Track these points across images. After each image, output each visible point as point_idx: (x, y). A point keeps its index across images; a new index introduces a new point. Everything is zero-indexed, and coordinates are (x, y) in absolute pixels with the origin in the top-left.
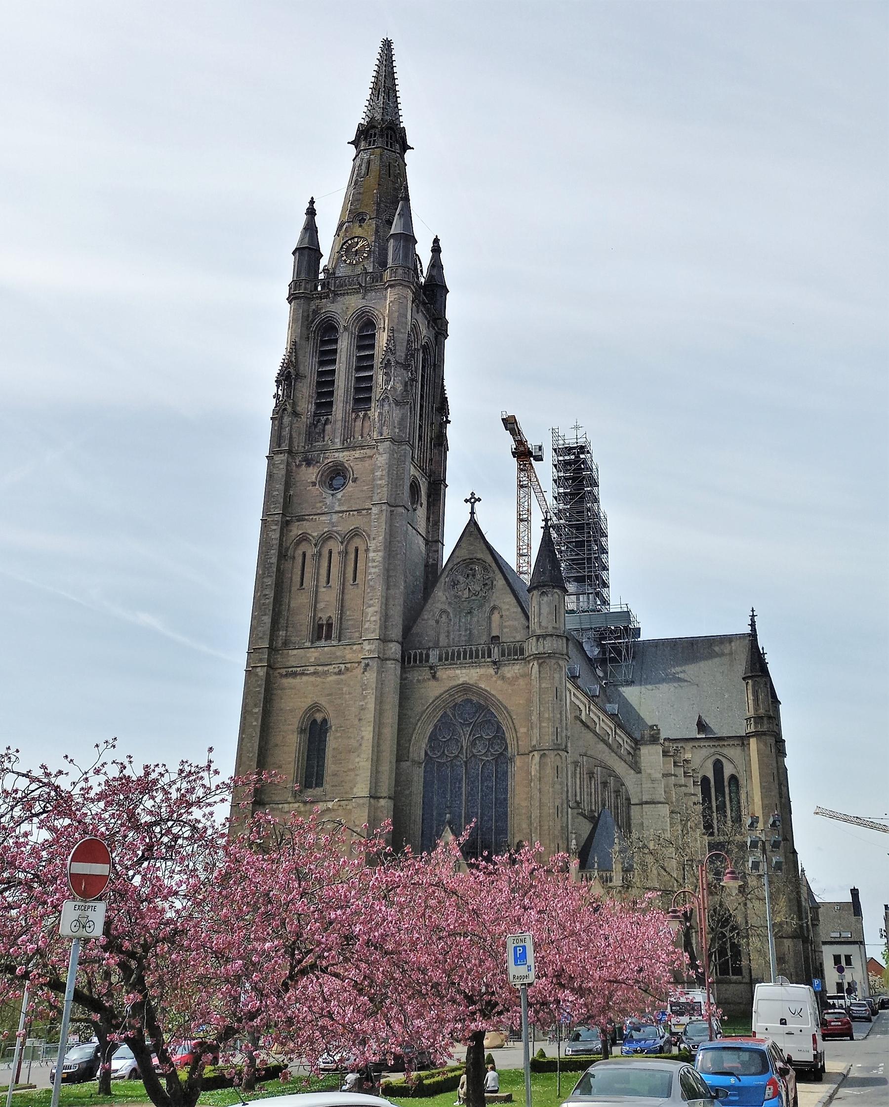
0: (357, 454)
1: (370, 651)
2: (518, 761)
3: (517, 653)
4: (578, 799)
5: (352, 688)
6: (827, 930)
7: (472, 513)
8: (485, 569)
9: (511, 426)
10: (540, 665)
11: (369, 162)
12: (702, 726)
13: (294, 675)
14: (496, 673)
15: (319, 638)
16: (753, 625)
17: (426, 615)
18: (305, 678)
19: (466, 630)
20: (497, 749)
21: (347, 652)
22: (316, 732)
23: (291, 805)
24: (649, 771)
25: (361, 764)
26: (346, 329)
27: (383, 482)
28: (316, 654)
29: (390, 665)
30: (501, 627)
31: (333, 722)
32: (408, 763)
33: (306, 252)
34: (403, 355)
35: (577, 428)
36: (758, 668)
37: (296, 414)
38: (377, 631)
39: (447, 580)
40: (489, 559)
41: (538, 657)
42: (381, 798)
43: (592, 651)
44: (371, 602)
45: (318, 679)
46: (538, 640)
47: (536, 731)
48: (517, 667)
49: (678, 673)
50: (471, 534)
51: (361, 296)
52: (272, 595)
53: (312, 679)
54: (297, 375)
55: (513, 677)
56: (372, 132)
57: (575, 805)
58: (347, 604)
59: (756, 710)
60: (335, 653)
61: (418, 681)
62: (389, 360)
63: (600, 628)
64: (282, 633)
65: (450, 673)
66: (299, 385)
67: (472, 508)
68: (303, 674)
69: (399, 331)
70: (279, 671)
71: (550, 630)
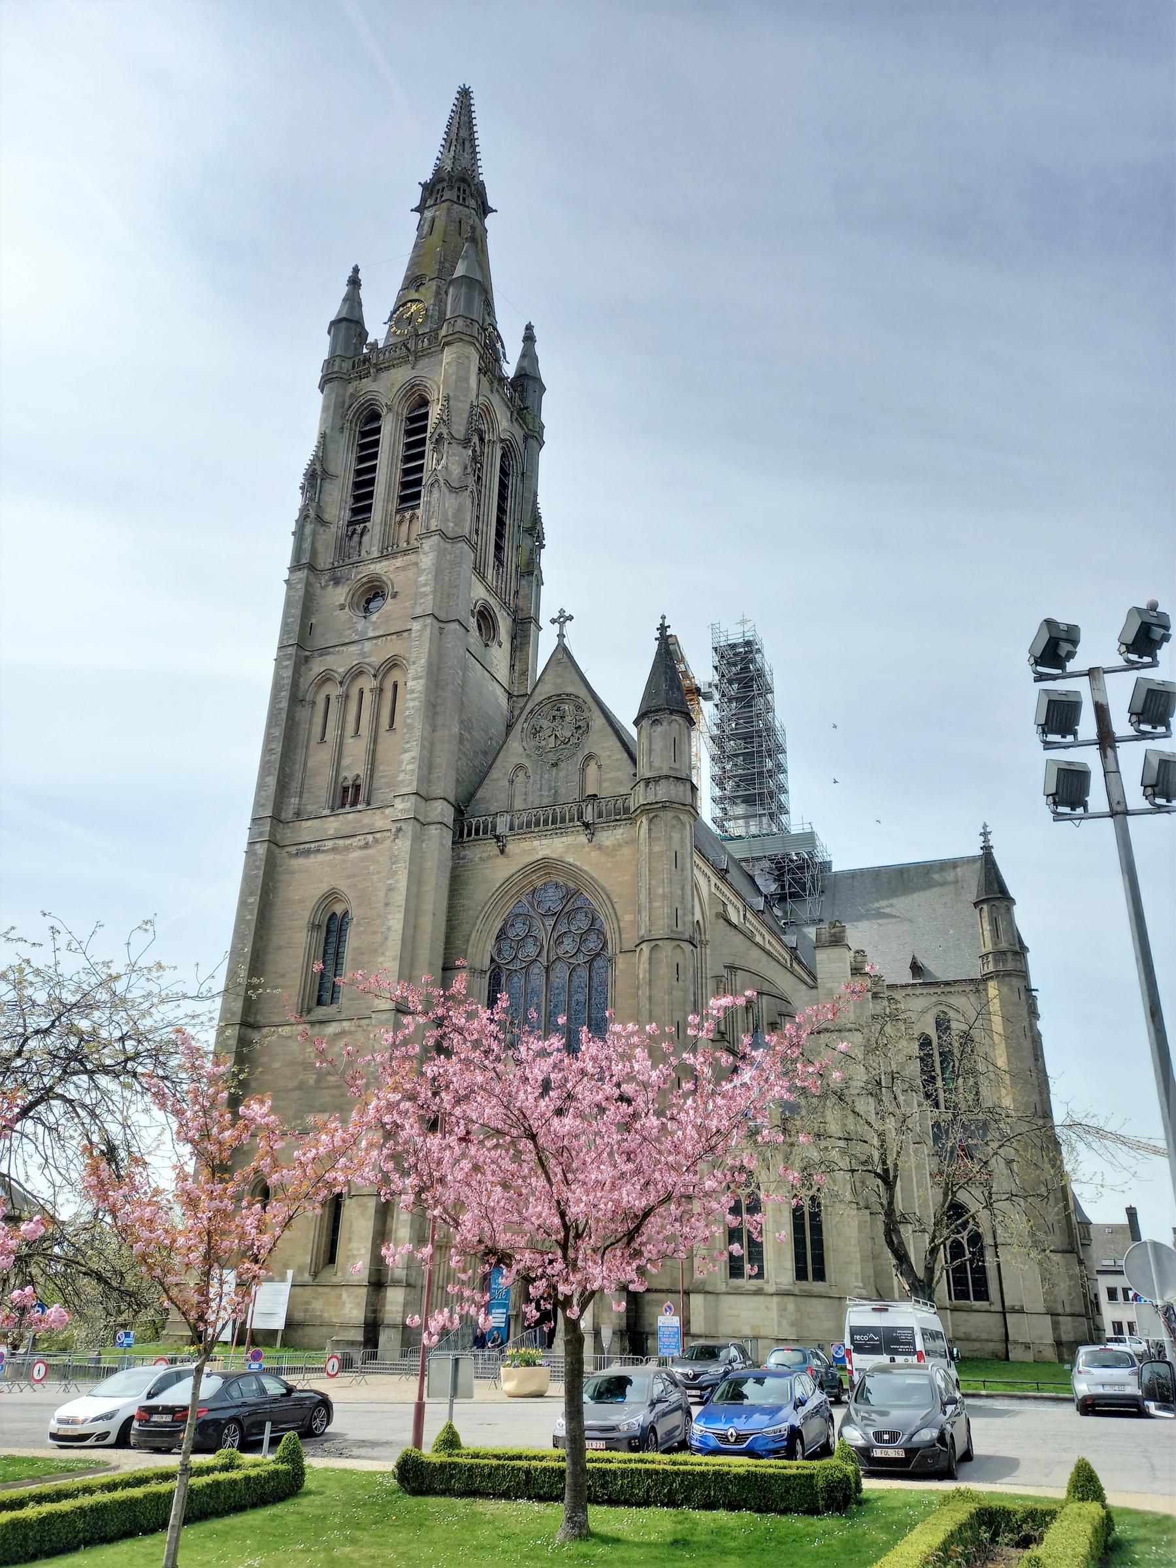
0: (399, 562)
1: (403, 811)
2: (621, 962)
3: (622, 814)
4: (722, 1028)
5: (382, 872)
6: (1100, 1256)
7: (561, 636)
8: (579, 708)
10: (651, 821)
11: (433, 220)
13: (308, 852)
14: (590, 841)
15: (343, 805)
17: (495, 774)
18: (321, 857)
19: (550, 790)
20: (593, 943)
21: (377, 818)
22: (332, 930)
23: (294, 1028)
24: (829, 985)
26: (390, 409)
27: (427, 589)
28: (336, 825)
29: (434, 830)
30: (600, 782)
31: (355, 913)
33: (343, 325)
34: (463, 430)
36: (994, 893)
37: (320, 520)
38: (415, 783)
39: (525, 725)
40: (583, 693)
41: (646, 809)
43: (767, 886)
44: (407, 746)
45: (338, 857)
46: (647, 785)
47: (645, 915)
48: (620, 831)
50: (559, 663)
51: (410, 366)
52: (280, 749)
53: (330, 857)
54: (324, 471)
56: (439, 186)
58: (379, 755)
59: (995, 944)
60: (360, 822)
62: (441, 434)
63: (776, 855)
64: (294, 801)
65: (526, 845)
66: (327, 486)
67: (561, 629)
71: (665, 772)
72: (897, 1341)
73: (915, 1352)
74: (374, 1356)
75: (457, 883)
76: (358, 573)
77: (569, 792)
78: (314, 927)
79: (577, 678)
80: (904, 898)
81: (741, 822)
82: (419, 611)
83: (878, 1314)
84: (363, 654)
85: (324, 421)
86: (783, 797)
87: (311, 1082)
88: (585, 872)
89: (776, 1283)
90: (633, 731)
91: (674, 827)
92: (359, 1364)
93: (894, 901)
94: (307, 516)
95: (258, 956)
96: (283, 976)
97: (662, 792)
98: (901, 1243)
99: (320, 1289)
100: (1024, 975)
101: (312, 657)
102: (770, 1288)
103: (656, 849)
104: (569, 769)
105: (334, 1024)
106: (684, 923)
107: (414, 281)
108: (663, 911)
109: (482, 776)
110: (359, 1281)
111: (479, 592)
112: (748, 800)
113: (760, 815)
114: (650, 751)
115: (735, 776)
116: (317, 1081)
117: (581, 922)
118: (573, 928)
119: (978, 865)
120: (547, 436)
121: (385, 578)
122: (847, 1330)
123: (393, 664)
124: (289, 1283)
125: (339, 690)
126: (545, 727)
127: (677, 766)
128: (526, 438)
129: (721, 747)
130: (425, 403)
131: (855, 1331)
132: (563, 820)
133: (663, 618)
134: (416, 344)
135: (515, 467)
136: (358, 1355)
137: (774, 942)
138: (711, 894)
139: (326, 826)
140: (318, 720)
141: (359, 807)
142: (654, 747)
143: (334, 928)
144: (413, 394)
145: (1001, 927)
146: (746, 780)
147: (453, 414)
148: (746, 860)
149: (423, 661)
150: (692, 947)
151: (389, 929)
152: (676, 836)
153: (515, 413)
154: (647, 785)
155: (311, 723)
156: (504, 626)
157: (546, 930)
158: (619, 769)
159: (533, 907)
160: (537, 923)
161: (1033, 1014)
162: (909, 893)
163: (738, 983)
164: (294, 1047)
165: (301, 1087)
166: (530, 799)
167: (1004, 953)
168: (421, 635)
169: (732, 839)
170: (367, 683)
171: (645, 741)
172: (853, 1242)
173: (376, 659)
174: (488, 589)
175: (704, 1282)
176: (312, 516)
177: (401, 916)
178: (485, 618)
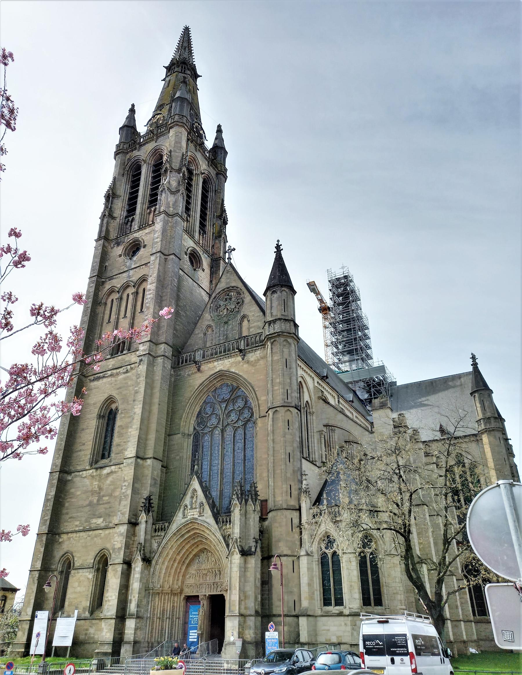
0: (147, 230)
1: (144, 350)
4: (324, 460)
8: (239, 293)
9: (313, 287)
10: (272, 344)
11: (170, 81)
12: (442, 431)
13: (99, 378)
14: (243, 359)
16: (475, 365)
17: (197, 331)
18: (105, 380)
19: (224, 336)
20: (246, 414)
21: (132, 357)
22: (109, 416)
23: (88, 472)
25: (132, 433)
27: (159, 240)
28: (113, 363)
30: (249, 329)
31: (120, 408)
32: (179, 436)
33: (125, 128)
34: (178, 165)
35: (343, 268)
36: (480, 387)
37: (114, 218)
38: (149, 336)
40: (240, 285)
41: (269, 337)
42: (148, 458)
44: (147, 317)
46: (269, 325)
48: (258, 352)
49: (423, 401)
52: (86, 327)
53: (109, 379)
55: (255, 360)
57: (321, 464)
59: (484, 414)
61: (189, 375)
65: (210, 365)
66: (115, 201)
68: (104, 377)
69: (175, 151)
70: (90, 378)
71: (279, 317)
72: (395, 645)
73: (407, 654)
74: (118, 662)
75: (174, 389)
76: (128, 239)
77: (233, 334)
78: (100, 417)
79: (237, 278)
80: (434, 395)
81: (347, 364)
82: (154, 251)
83: (381, 625)
84: (129, 277)
85: (115, 171)
86: (369, 351)
87: (95, 501)
88: (241, 376)
89: (350, 608)
90: (264, 298)
91: (285, 346)
92: (109, 667)
93: (429, 398)
94: (105, 215)
95: (71, 435)
96: (84, 444)
97: (277, 327)
98: (419, 578)
99: (94, 621)
100: (503, 431)
101: (105, 281)
102: (347, 612)
103: (275, 358)
104: (234, 323)
105: (107, 468)
106: (292, 397)
107: (160, 107)
108: (279, 391)
109: (190, 333)
110: (111, 615)
111: (189, 243)
112: (350, 352)
113: (357, 360)
114: (271, 307)
115: (342, 341)
116: (98, 501)
117: (240, 403)
118: (236, 407)
119: (471, 376)
120: (228, 174)
121: (140, 239)
122: (361, 638)
123: (143, 279)
124: (75, 618)
125: (117, 296)
126: (222, 305)
127: (286, 314)
128: (217, 174)
129: (335, 328)
130: (161, 156)
131: (367, 638)
132: (229, 350)
133: (278, 241)
134: (157, 131)
135: (212, 187)
136: (108, 661)
137: (359, 417)
138: (315, 387)
139: (108, 364)
140: (107, 312)
141: (124, 352)
142: (273, 305)
143: (111, 417)
144: (156, 154)
145: (486, 404)
146: (349, 342)
147: (173, 158)
148: (351, 383)
149: (155, 274)
150: (297, 411)
151: (135, 413)
152: (286, 350)
153: (210, 162)
154: (269, 325)
155: (104, 314)
156: (206, 262)
157: (221, 409)
158: (258, 321)
159: (215, 398)
160: (217, 406)
161: (510, 453)
162: (436, 393)
163: (336, 437)
164: (87, 482)
165: (91, 504)
166: (213, 342)
167: (489, 418)
168: (155, 261)
169: (343, 372)
170: (131, 290)
171: (269, 302)
172: (397, 581)
173: (135, 279)
174: (197, 243)
175: (307, 609)
176: (108, 214)
177: (141, 406)
178: (194, 258)
